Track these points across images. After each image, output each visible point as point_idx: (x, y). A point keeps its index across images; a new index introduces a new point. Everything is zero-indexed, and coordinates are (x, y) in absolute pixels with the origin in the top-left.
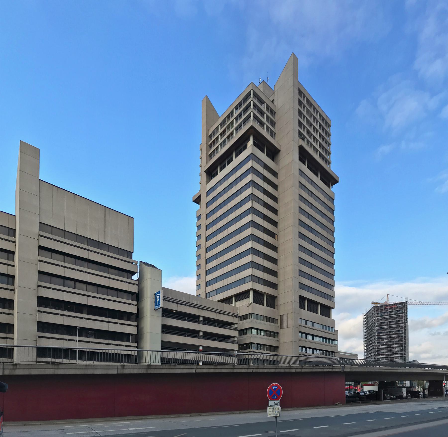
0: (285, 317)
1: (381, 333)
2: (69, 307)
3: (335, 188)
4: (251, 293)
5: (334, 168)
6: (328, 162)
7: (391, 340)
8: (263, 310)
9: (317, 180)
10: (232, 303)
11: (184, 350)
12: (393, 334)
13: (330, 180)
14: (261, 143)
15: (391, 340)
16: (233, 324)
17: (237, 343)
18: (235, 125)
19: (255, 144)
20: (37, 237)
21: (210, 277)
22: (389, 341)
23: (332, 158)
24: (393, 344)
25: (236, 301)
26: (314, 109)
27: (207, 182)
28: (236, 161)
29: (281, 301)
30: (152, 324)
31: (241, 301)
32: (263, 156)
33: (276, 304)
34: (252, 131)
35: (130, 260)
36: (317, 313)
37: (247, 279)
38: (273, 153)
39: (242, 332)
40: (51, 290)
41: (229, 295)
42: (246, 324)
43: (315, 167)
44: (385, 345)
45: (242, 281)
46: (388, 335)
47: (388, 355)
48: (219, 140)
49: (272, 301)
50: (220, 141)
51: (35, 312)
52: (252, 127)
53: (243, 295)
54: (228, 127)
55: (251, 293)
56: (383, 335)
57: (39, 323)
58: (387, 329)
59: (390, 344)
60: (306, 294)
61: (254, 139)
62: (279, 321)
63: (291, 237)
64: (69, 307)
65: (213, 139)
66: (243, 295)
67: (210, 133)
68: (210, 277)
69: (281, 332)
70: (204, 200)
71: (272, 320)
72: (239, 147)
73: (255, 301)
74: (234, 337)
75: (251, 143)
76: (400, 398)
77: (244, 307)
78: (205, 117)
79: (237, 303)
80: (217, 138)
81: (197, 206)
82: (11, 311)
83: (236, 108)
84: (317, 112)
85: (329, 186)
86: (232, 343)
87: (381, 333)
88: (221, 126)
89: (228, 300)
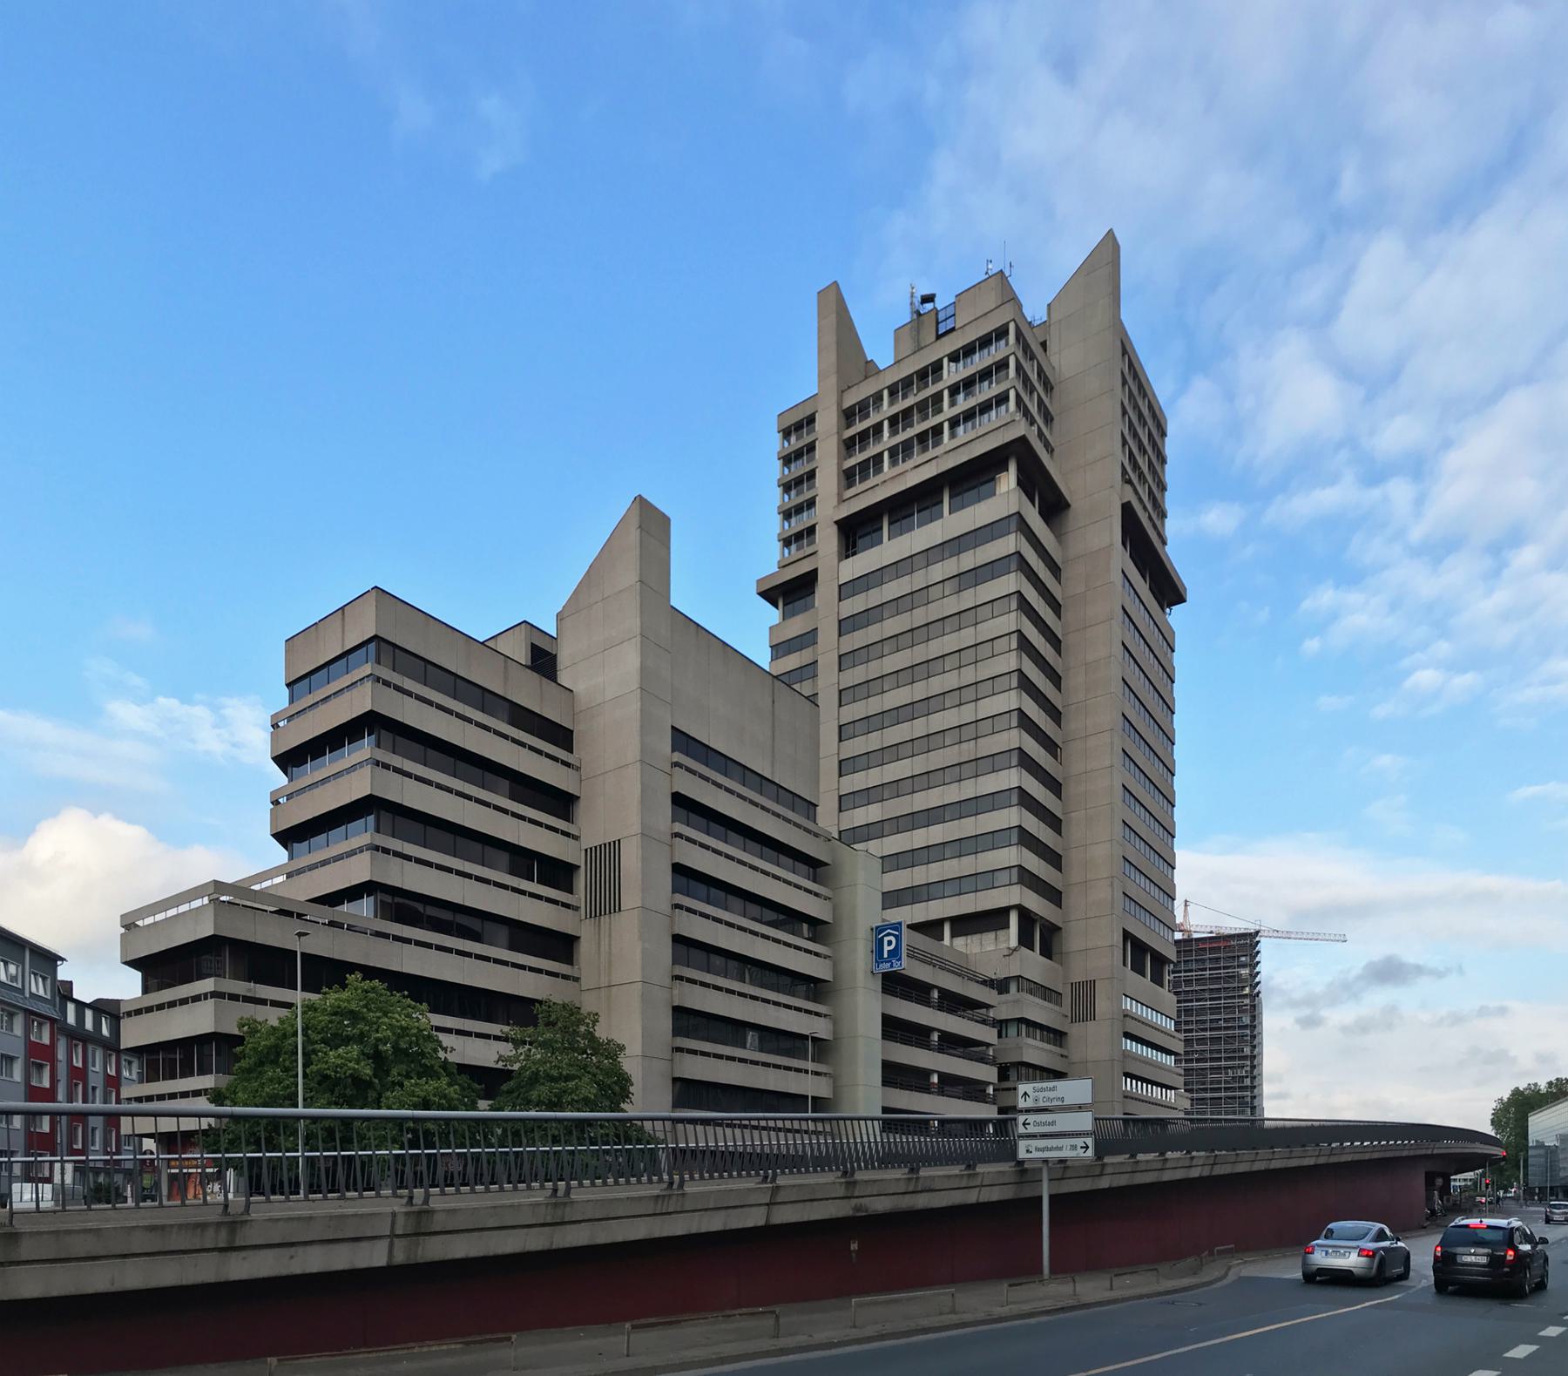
1: (1186, 1023)
3: (1176, 617)
4: (1014, 918)
7: (1216, 1047)
8: (1032, 964)
9: (1143, 587)
12: (1219, 1029)
13: (1168, 591)
14: (1037, 483)
15: (1216, 1047)
16: (988, 1007)
17: (993, 1063)
18: (948, 412)
20: (668, 768)
22: (1207, 1047)
24: (1219, 1059)
25: (953, 936)
26: (1140, 387)
29: (1074, 941)
30: (866, 1007)
31: (976, 937)
33: (1055, 949)
34: (1019, 451)
35: (810, 825)
37: (1003, 878)
38: (1054, 506)
39: (1001, 1025)
42: (1004, 1007)
44: (1198, 1060)
45: (983, 880)
46: (1205, 1030)
47: (1205, 1090)
48: (886, 433)
50: (888, 440)
52: (1023, 440)
53: (992, 920)
54: (922, 407)
55: (1014, 918)
56: (1191, 1031)
58: (1202, 1011)
59: (1212, 1060)
61: (1020, 470)
62: (1067, 1000)
63: (1108, 763)
66: (992, 920)
69: (1075, 1031)
71: (1046, 993)
72: (971, 478)
73: (1025, 940)
74: (988, 1045)
75: (1008, 481)
77: (993, 952)
78: (834, 347)
80: (878, 428)
84: (1145, 395)
86: (984, 1022)
87: (1186, 1023)
89: (931, 928)
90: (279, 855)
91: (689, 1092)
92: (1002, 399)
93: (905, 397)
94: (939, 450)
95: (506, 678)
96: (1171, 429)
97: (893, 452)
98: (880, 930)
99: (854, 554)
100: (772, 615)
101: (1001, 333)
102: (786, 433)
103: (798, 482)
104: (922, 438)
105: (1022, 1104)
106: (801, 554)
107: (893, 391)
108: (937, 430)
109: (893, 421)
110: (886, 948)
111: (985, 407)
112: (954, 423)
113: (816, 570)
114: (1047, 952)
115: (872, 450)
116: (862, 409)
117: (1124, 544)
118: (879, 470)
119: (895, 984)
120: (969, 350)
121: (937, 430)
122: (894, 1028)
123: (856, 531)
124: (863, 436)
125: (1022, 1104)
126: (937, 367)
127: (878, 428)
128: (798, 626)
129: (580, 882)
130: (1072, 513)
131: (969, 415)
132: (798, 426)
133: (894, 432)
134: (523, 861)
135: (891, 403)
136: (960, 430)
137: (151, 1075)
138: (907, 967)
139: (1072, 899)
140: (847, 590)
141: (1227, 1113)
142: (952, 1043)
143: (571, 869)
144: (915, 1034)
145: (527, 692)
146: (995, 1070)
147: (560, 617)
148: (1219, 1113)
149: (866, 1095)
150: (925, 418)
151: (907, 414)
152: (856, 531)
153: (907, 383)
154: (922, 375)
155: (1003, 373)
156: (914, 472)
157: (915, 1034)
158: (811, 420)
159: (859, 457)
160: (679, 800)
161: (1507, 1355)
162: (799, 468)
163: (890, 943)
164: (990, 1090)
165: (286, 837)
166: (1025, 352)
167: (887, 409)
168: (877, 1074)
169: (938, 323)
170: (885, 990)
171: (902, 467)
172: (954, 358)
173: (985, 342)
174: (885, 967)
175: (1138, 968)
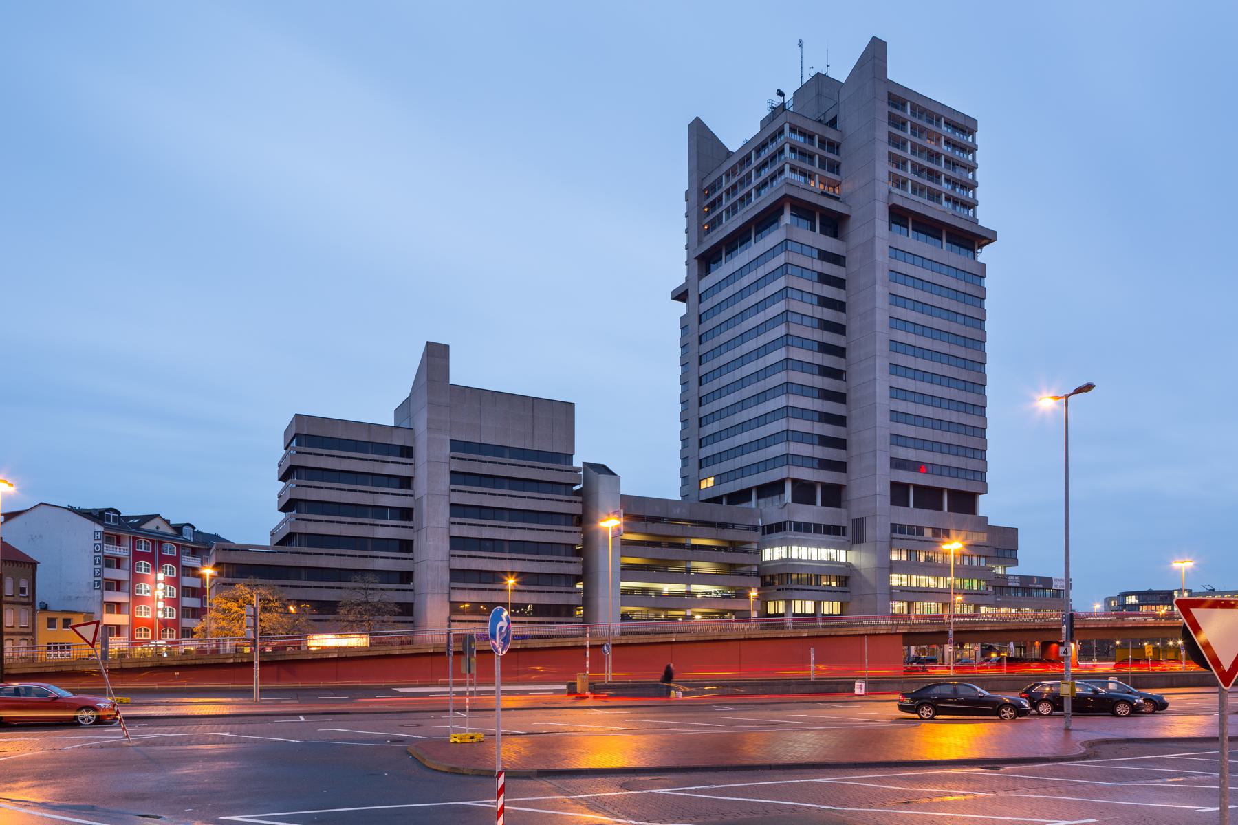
3: (985, 255)
4: (788, 487)
5: (985, 217)
10: (751, 499)
11: (836, 692)
18: (755, 181)
25: (759, 497)
27: (700, 277)
29: (854, 493)
38: (834, 224)
41: (745, 487)
43: (929, 227)
49: (834, 496)
50: (726, 204)
51: (446, 558)
53: (771, 489)
54: (741, 182)
55: (788, 487)
57: (452, 570)
60: (904, 477)
62: (849, 531)
65: (711, 198)
67: (705, 185)
70: (693, 297)
75: (787, 211)
79: (762, 501)
81: (681, 308)
82: (410, 555)
83: (758, 151)
88: (728, 176)
92: (486, 622)
94: (750, 206)
104: (741, 200)
108: (749, 194)
109: (728, 192)
112: (758, 189)
116: (713, 188)
118: (721, 223)
130: (851, 220)
131: (765, 184)
133: (728, 199)
136: (762, 192)
141: (456, 684)
148: (463, 684)
151: (734, 187)
161: (12, 490)
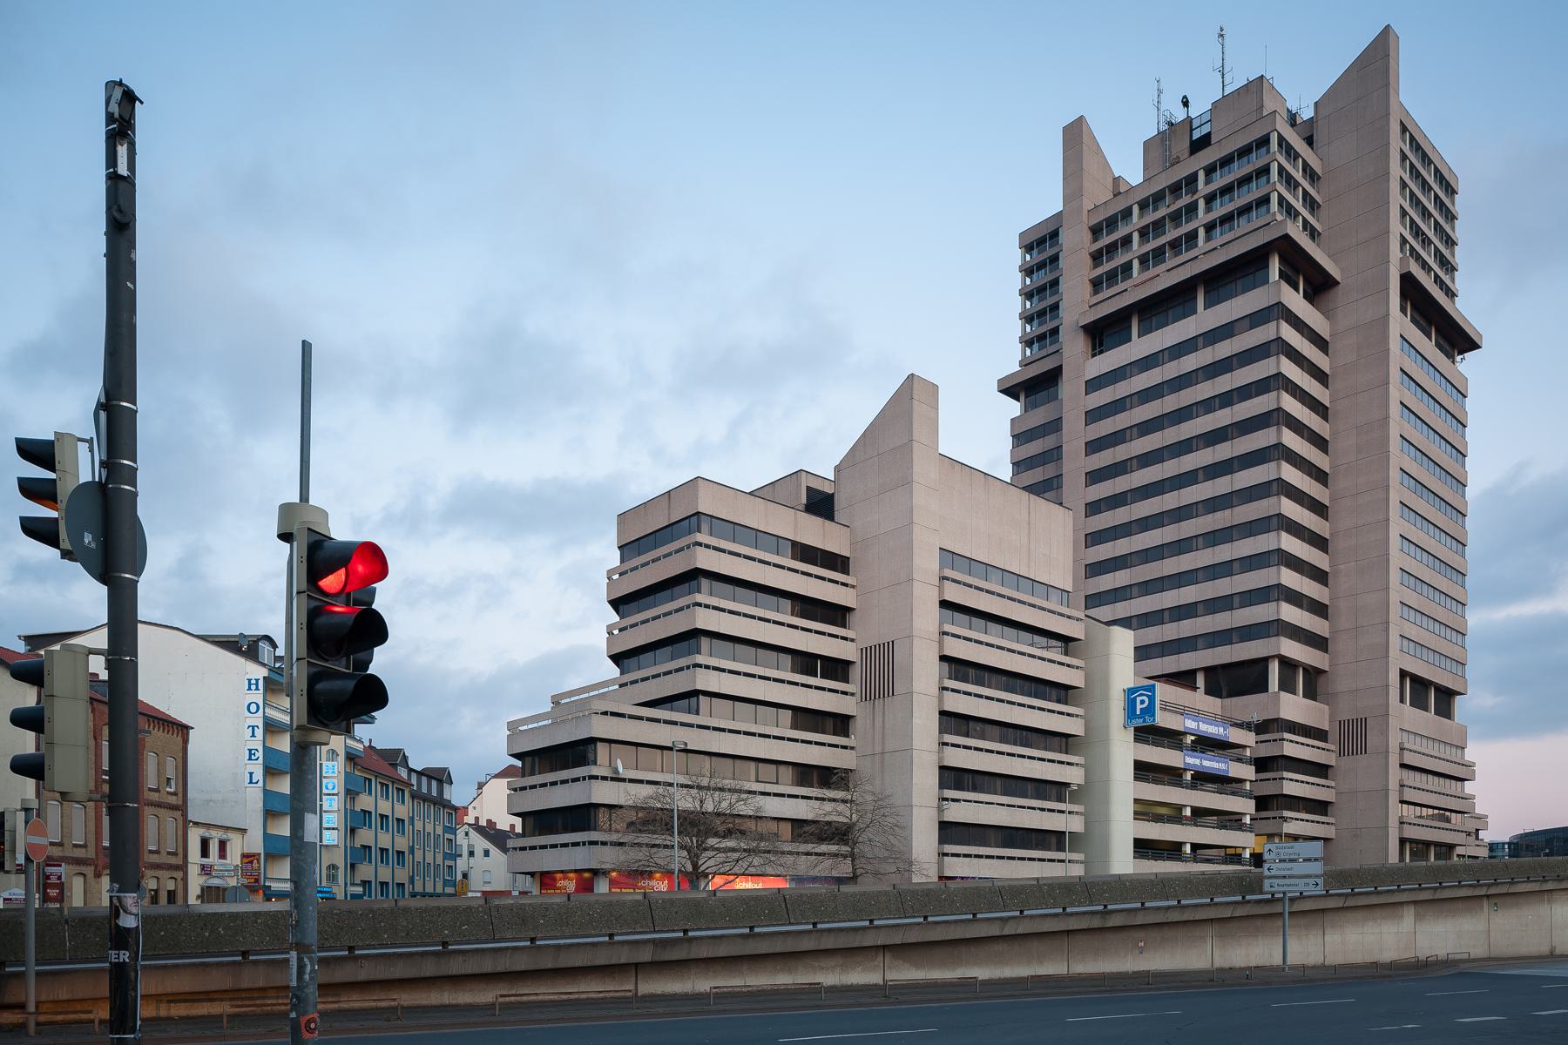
0: (883, 658)
2: (88, 538)
3: (1468, 364)
5: (1468, 307)
6: (1451, 294)
9: (1428, 346)
13: (1457, 340)
19: (1282, 275)
21: (1107, 582)
23: (1460, 283)
28: (1205, 318)
29: (1342, 683)
32: (1295, 301)
36: (1426, 709)
40: (813, 579)
54: (1175, 217)
61: (1282, 260)
64: (88, 538)
68: (1107, 582)
74: (1244, 747)
76: (351, 794)
85: (1451, 357)
86: (1239, 760)
90: (613, 671)
91: (950, 831)
93: (1155, 209)
95: (796, 527)
96: (1462, 187)
97: (1144, 260)
98: (1131, 691)
99: (1101, 352)
100: (1014, 408)
101: (1264, 142)
102: (1028, 248)
103: (1041, 290)
104: (1175, 245)
105: (1267, 873)
106: (1043, 352)
107: (1143, 205)
109: (1143, 233)
110: (1139, 707)
111: (1245, 210)
113: (1060, 367)
114: (1311, 693)
115: (1120, 259)
117: (1403, 310)
119: (1148, 734)
120: (1226, 161)
121: (1192, 237)
122: (1144, 770)
123: (1102, 333)
124: (1111, 249)
125: (1267, 873)
126: (1192, 179)
127: (1127, 241)
128: (1040, 416)
129: (855, 673)
131: (1227, 219)
132: (1042, 246)
134: (806, 662)
135: (1141, 216)
137: (796, 837)
138: (1163, 720)
139: (1341, 646)
140: (1093, 385)
142: (1203, 779)
143: (847, 664)
144: (1170, 775)
145: (814, 532)
146: (1253, 802)
147: (838, 469)
149: (1123, 829)
150: (1178, 226)
152: (1102, 333)
153: (1158, 198)
154: (1175, 189)
155: (1264, 209)
156: (1166, 277)
157: (1170, 775)
158: (1055, 234)
159: (1107, 267)
160: (945, 604)
162: (1042, 277)
163: (1142, 702)
164: (1247, 820)
165: (617, 658)
166: (1288, 154)
167: (1137, 221)
168: (1130, 809)
169: (1192, 130)
170: (1137, 740)
171: (1152, 272)
172: (1210, 170)
173: (1245, 152)
174: (1139, 722)
175: (1419, 702)
